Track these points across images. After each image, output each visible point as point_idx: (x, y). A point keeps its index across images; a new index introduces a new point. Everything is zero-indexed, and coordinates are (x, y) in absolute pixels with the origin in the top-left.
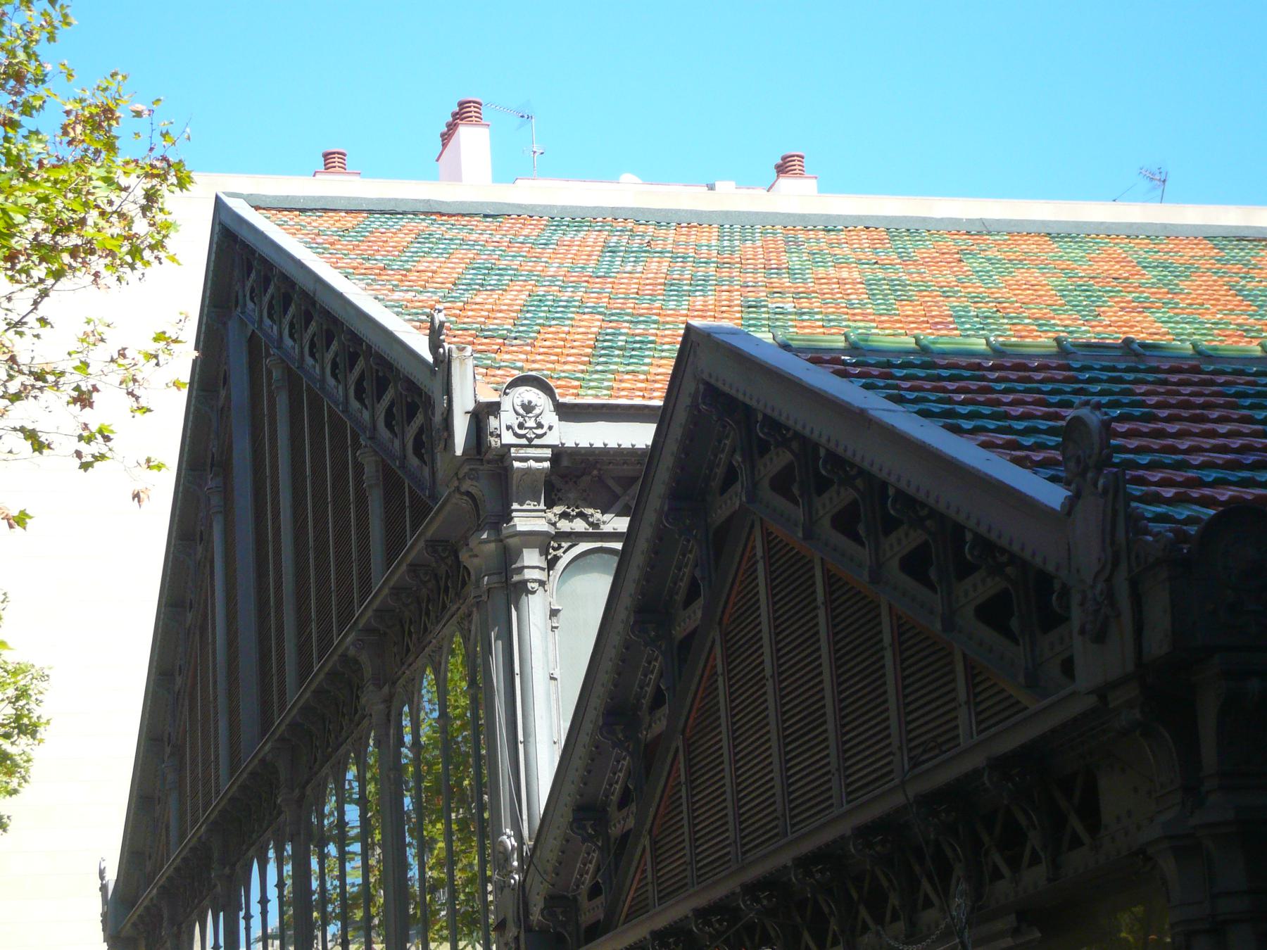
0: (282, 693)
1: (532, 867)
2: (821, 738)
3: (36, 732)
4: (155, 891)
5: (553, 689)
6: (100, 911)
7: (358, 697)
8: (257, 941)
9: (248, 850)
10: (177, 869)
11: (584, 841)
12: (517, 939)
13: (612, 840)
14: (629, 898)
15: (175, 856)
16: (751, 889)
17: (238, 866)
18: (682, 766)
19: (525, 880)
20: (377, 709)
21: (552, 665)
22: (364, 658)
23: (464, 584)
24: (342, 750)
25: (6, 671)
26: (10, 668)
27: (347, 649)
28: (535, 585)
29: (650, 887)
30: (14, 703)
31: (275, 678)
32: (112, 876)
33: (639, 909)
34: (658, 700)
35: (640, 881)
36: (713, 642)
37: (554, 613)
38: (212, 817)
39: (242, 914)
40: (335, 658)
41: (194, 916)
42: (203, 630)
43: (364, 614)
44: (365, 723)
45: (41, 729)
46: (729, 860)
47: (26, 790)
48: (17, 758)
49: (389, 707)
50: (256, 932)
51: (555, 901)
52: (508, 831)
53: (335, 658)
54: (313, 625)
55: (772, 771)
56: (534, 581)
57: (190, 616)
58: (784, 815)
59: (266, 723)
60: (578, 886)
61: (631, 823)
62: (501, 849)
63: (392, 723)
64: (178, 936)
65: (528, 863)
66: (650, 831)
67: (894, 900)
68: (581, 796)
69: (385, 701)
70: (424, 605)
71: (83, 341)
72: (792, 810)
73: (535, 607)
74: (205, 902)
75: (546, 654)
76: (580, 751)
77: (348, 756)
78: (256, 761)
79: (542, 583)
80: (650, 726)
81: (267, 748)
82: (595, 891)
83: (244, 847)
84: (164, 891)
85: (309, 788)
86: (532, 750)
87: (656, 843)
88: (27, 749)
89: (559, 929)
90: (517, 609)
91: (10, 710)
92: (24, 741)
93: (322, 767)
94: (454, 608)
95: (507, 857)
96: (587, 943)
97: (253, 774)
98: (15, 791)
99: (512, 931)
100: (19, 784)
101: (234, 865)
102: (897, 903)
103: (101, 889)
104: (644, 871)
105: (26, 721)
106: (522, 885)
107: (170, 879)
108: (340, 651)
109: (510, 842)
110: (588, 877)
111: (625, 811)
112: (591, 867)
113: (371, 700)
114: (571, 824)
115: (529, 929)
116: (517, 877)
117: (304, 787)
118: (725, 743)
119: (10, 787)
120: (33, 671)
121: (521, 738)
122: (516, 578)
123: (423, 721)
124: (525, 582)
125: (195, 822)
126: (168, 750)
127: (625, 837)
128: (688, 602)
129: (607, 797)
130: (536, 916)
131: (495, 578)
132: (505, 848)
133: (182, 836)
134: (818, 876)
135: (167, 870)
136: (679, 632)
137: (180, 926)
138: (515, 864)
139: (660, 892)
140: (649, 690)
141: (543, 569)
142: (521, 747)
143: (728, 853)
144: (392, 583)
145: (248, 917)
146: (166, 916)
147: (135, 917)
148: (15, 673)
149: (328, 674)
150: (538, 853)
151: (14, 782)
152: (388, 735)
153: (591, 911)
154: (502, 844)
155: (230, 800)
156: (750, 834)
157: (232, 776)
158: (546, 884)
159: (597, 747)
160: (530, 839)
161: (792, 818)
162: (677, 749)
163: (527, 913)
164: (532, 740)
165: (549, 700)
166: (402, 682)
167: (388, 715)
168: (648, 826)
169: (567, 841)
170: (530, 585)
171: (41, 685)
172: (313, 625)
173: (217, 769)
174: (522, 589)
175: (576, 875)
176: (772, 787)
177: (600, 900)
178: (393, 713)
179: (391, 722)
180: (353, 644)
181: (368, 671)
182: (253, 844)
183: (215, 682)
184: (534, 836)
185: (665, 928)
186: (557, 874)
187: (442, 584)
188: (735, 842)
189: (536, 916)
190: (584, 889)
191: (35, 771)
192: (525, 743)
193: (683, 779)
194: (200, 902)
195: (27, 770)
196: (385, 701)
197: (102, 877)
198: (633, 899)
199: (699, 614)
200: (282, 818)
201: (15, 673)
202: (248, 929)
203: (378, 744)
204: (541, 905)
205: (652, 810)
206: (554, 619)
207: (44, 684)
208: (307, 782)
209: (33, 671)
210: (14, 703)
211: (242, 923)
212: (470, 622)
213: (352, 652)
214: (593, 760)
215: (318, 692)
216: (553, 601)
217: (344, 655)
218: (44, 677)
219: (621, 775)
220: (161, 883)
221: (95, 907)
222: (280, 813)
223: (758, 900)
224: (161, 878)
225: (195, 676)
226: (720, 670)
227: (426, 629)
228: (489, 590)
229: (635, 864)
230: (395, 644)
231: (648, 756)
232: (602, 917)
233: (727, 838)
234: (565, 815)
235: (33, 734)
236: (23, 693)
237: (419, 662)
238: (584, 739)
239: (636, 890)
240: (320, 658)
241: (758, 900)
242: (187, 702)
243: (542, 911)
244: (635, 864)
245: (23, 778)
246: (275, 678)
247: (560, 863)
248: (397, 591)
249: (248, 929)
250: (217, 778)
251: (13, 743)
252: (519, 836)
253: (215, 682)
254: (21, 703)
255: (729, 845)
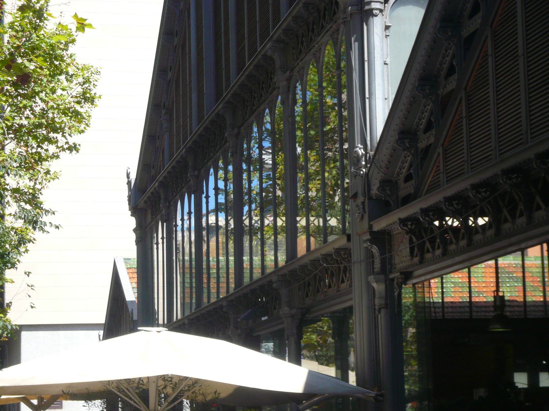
0: (228, 79)
1: (373, 165)
2: (487, 125)
3: (93, 101)
4: (157, 184)
5: (385, 70)
6: (127, 195)
7: (271, 79)
8: (213, 211)
9: (208, 162)
10: (169, 173)
11: (404, 150)
12: (363, 203)
13: (420, 150)
14: (429, 182)
15: (168, 166)
16: (507, 173)
17: (202, 170)
18: (464, 108)
19: (368, 172)
20: (283, 84)
21: (385, 56)
22: (276, 57)
23: (335, 13)
24: (262, 107)
25: (78, 69)
26: (80, 67)
27: (267, 51)
28: (378, 12)
29: (441, 175)
30: (82, 86)
31: (224, 71)
32: (133, 177)
33: (434, 187)
34: (451, 71)
35: (435, 172)
36: (487, 37)
37: (387, 28)
38: (189, 145)
39: (204, 196)
40: (260, 57)
41: (178, 197)
42: (183, 47)
43: (276, 33)
44: (275, 92)
45: (96, 100)
46: (491, 159)
47: (88, 131)
48: (84, 115)
49: (289, 84)
50: (212, 206)
51: (385, 183)
52: (359, 145)
53: (260, 57)
54: (246, 41)
55: (520, 108)
56: (377, 9)
57: (176, 40)
58: (527, 132)
59: (218, 95)
60: (398, 175)
61: (432, 140)
62: (356, 155)
63: (291, 93)
64: (169, 207)
65: (371, 161)
66: (443, 145)
67: (521, 207)
68: (403, 125)
69: (287, 80)
70: (253, 94)
71: (71, 56)
72: (531, 129)
73: (377, 24)
74: (184, 190)
75: (382, 50)
76: (404, 100)
77: (220, 156)
78: (214, 114)
79: (381, 11)
80: (445, 86)
81: (220, 107)
82: (408, 178)
83: (206, 161)
84: (162, 184)
85: (242, 128)
86: (373, 102)
87: (446, 151)
88: (89, 110)
89: (388, 199)
90: (367, 25)
91: (80, 89)
92: (87, 105)
93: (250, 117)
94: (329, 27)
95: (358, 159)
96: (402, 206)
97: (178, 162)
98: (83, 131)
99: (360, 199)
100: (85, 128)
101: (200, 170)
102: (522, 207)
103: (127, 184)
104: (438, 166)
105: (88, 95)
106: (367, 174)
107: (165, 177)
108: (262, 53)
109: (361, 152)
110: (404, 171)
111: (428, 134)
112: (407, 165)
113: (280, 79)
114: (397, 141)
115: (370, 198)
116: (364, 170)
117: (239, 128)
118: (491, 94)
119: (80, 129)
120: (92, 69)
121: (367, 96)
122: (367, 7)
123: (306, 94)
124: (372, 9)
125: (178, 149)
126: (164, 111)
127: (427, 150)
128: (471, 16)
129: (418, 126)
130: (375, 190)
131: (355, 8)
132: (358, 155)
133: (171, 156)
134: (483, 194)
135: (163, 173)
136: (465, 33)
137: (170, 202)
138: (364, 163)
139: (447, 177)
140: (445, 66)
141: (381, 3)
142: (367, 101)
143: (491, 155)
144: (293, 14)
145: (207, 197)
146: (162, 196)
147: (146, 198)
148: (83, 70)
149: (254, 66)
150: (377, 157)
151: (82, 126)
152: (288, 98)
153: (406, 189)
154: (356, 152)
155: (193, 141)
156: (536, 127)
157: (199, 124)
158: (381, 173)
159: (414, 98)
160: (371, 150)
161: (532, 134)
162: (461, 98)
163: (369, 189)
164: (373, 97)
165: (383, 75)
166: (297, 69)
167: (289, 87)
168: (441, 142)
169: (394, 150)
170: (374, 12)
171: (96, 77)
172: (246, 41)
173: (191, 120)
174: (370, 13)
175: (398, 170)
176: (520, 117)
177: (412, 182)
178: (291, 86)
179: (290, 91)
180: (270, 49)
181: (278, 64)
182: (211, 159)
183: (190, 74)
184: (374, 149)
185: (407, 217)
186: (387, 168)
187: (311, 27)
188: (495, 148)
189: (375, 190)
190: (402, 177)
191: (93, 122)
192: (370, 98)
193: (464, 115)
194: (181, 189)
195: (89, 121)
196: (287, 80)
197: (128, 177)
198: (431, 182)
199: (479, 21)
200: (227, 144)
201: (83, 70)
202: (207, 203)
203: (283, 103)
204: (378, 185)
205: (444, 133)
206: (387, 31)
207: (98, 76)
208: (242, 126)
209: (92, 69)
210: (82, 86)
211: (204, 200)
212: (338, 34)
213: (269, 53)
214: (411, 105)
215: (206, 129)
216: (387, 21)
217: (265, 56)
218: (98, 73)
219: (426, 114)
220: (160, 180)
221: (124, 193)
222: (226, 142)
223: (452, 205)
224: (160, 178)
225: (179, 71)
226: (490, 53)
227: (311, 39)
228: (351, 14)
229: (433, 162)
230: (293, 48)
231: (444, 104)
232: (412, 191)
233: (490, 146)
234: (394, 135)
235: (92, 102)
236: (87, 81)
237: (307, 58)
238: (407, 93)
239: (434, 177)
240: (190, 135)
241: (452, 205)
242: (174, 86)
243: (378, 188)
244: (433, 162)
245: (87, 125)
246: (224, 71)
247: (389, 162)
248: (296, 19)
249: (207, 203)
250: (191, 125)
251: (82, 107)
252: (365, 148)
253: (190, 74)
254: (86, 86)
255: (490, 151)
